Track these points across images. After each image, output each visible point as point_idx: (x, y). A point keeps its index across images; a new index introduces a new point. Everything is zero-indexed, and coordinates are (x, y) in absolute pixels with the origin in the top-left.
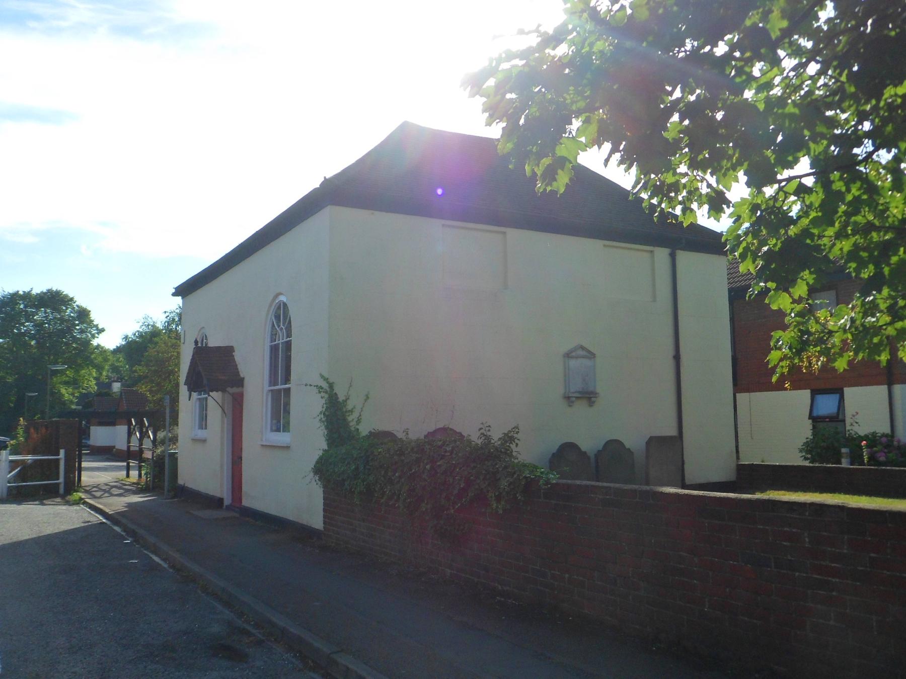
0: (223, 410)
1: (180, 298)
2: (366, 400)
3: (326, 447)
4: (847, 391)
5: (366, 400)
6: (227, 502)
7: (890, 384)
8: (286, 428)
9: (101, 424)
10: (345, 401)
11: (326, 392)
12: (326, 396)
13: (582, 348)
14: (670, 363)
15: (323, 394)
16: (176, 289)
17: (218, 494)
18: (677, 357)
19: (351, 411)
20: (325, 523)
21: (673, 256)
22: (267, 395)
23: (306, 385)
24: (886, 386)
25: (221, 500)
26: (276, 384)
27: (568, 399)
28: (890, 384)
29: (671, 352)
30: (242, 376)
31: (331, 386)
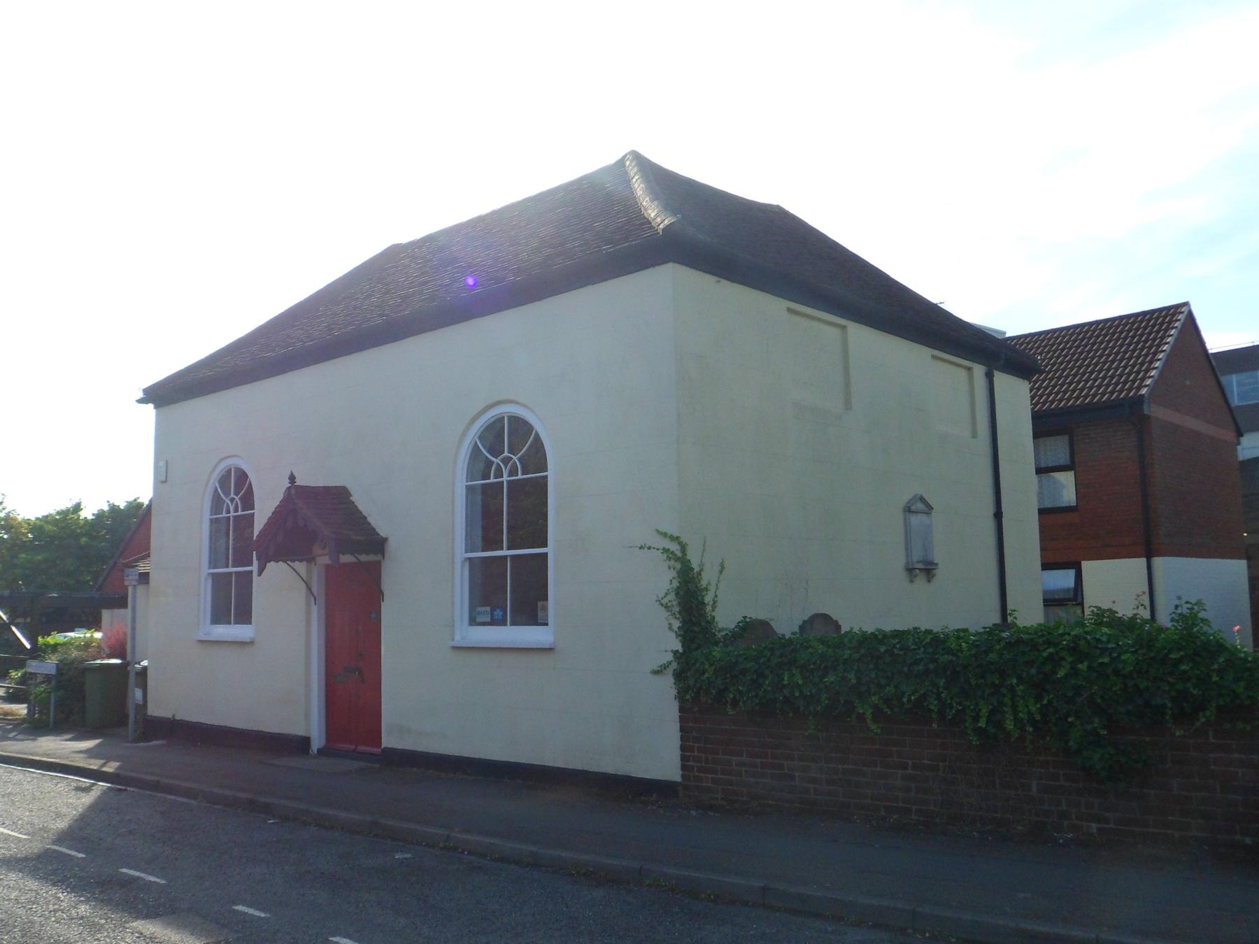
0: (309, 588)
1: (151, 406)
2: (721, 572)
3: (678, 647)
4: (1086, 565)
5: (721, 572)
6: (317, 742)
7: (1149, 558)
8: (244, 616)
9: (108, 608)
10: (699, 573)
11: (677, 559)
12: (678, 566)
13: (922, 499)
14: (990, 523)
15: (672, 563)
16: (146, 391)
17: (299, 730)
18: (998, 515)
19: (706, 589)
20: (684, 768)
21: (989, 376)
22: (463, 566)
23: (641, 548)
24: (1144, 560)
25: (305, 742)
26: (491, 542)
27: (910, 570)
28: (1149, 558)
29: (991, 510)
30: (383, 534)
31: (683, 548)
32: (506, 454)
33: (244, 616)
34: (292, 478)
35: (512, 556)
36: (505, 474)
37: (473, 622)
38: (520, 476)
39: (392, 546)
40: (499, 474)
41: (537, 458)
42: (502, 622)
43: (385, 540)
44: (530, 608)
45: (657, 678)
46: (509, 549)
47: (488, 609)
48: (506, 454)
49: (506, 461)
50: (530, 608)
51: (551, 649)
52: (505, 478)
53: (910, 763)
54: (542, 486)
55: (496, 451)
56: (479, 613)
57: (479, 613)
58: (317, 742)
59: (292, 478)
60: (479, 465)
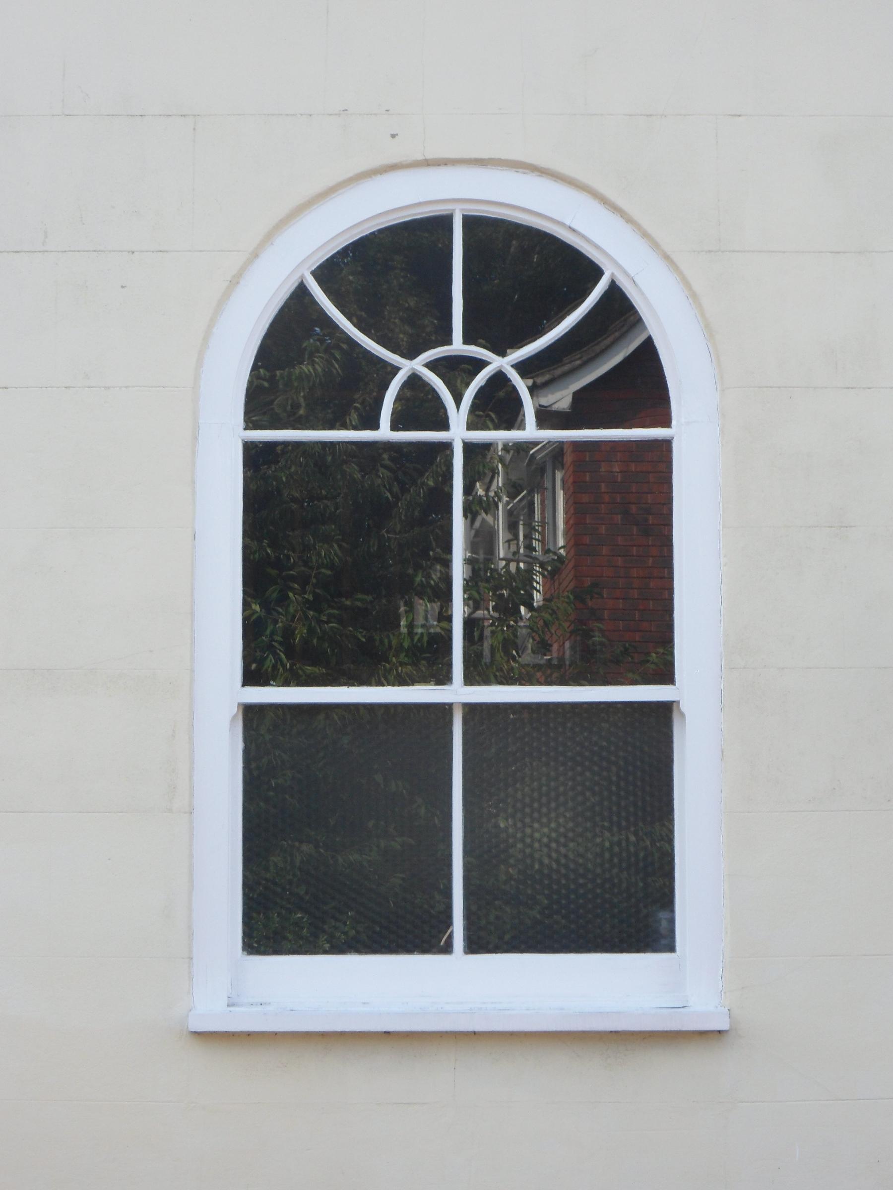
35: (472, 710)
36: (458, 418)
40: (420, 408)
52: (458, 431)
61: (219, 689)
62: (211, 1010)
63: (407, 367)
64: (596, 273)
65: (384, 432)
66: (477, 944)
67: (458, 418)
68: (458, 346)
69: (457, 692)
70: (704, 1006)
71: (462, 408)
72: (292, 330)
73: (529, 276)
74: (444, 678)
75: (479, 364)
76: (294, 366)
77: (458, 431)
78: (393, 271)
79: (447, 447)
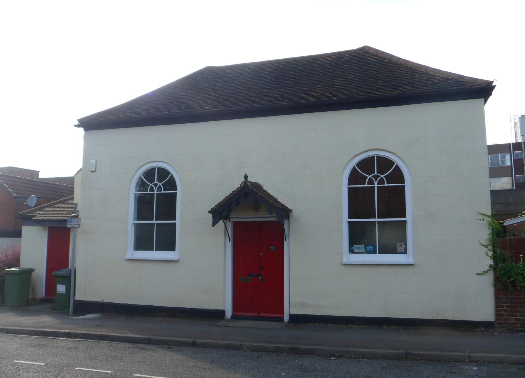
3: (492, 262)
8: (171, 247)
17: (220, 307)
25: (219, 314)
32: (376, 173)
33: (171, 247)
34: (246, 177)
35: (157, 224)
36: (155, 190)
37: (351, 251)
38: (163, 192)
39: (296, 213)
40: (152, 189)
41: (172, 184)
42: (374, 252)
43: (291, 211)
44: (168, 242)
45: (482, 278)
46: (156, 220)
47: (363, 246)
48: (156, 182)
49: (376, 177)
50: (168, 242)
51: (178, 261)
52: (376, 185)
53: (505, 308)
54: (174, 197)
55: (152, 181)
56: (356, 248)
57: (356, 248)
58: (229, 314)
59: (246, 177)
60: (141, 185)
61: (345, 219)
62: (128, 256)
63: (369, 177)
64: (170, 173)
65: (148, 192)
66: (156, 250)
67: (155, 190)
68: (156, 182)
69: (376, 219)
70: (410, 261)
71: (376, 182)
72: (354, 172)
73: (385, 163)
74: (153, 220)
75: (158, 184)
76: (355, 177)
77: (376, 185)
78: (366, 164)
79: (375, 187)
